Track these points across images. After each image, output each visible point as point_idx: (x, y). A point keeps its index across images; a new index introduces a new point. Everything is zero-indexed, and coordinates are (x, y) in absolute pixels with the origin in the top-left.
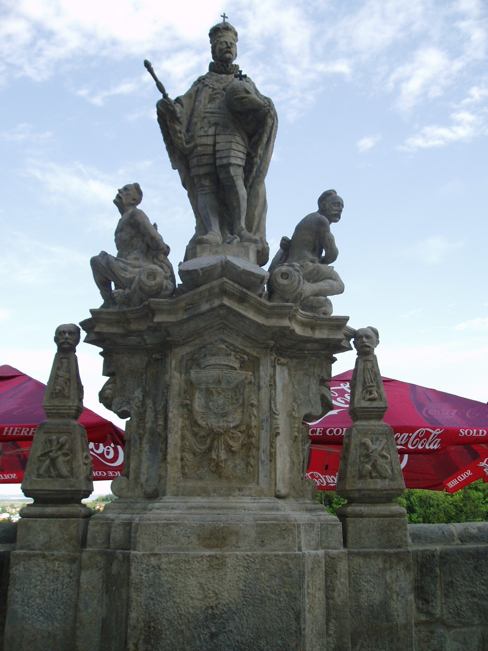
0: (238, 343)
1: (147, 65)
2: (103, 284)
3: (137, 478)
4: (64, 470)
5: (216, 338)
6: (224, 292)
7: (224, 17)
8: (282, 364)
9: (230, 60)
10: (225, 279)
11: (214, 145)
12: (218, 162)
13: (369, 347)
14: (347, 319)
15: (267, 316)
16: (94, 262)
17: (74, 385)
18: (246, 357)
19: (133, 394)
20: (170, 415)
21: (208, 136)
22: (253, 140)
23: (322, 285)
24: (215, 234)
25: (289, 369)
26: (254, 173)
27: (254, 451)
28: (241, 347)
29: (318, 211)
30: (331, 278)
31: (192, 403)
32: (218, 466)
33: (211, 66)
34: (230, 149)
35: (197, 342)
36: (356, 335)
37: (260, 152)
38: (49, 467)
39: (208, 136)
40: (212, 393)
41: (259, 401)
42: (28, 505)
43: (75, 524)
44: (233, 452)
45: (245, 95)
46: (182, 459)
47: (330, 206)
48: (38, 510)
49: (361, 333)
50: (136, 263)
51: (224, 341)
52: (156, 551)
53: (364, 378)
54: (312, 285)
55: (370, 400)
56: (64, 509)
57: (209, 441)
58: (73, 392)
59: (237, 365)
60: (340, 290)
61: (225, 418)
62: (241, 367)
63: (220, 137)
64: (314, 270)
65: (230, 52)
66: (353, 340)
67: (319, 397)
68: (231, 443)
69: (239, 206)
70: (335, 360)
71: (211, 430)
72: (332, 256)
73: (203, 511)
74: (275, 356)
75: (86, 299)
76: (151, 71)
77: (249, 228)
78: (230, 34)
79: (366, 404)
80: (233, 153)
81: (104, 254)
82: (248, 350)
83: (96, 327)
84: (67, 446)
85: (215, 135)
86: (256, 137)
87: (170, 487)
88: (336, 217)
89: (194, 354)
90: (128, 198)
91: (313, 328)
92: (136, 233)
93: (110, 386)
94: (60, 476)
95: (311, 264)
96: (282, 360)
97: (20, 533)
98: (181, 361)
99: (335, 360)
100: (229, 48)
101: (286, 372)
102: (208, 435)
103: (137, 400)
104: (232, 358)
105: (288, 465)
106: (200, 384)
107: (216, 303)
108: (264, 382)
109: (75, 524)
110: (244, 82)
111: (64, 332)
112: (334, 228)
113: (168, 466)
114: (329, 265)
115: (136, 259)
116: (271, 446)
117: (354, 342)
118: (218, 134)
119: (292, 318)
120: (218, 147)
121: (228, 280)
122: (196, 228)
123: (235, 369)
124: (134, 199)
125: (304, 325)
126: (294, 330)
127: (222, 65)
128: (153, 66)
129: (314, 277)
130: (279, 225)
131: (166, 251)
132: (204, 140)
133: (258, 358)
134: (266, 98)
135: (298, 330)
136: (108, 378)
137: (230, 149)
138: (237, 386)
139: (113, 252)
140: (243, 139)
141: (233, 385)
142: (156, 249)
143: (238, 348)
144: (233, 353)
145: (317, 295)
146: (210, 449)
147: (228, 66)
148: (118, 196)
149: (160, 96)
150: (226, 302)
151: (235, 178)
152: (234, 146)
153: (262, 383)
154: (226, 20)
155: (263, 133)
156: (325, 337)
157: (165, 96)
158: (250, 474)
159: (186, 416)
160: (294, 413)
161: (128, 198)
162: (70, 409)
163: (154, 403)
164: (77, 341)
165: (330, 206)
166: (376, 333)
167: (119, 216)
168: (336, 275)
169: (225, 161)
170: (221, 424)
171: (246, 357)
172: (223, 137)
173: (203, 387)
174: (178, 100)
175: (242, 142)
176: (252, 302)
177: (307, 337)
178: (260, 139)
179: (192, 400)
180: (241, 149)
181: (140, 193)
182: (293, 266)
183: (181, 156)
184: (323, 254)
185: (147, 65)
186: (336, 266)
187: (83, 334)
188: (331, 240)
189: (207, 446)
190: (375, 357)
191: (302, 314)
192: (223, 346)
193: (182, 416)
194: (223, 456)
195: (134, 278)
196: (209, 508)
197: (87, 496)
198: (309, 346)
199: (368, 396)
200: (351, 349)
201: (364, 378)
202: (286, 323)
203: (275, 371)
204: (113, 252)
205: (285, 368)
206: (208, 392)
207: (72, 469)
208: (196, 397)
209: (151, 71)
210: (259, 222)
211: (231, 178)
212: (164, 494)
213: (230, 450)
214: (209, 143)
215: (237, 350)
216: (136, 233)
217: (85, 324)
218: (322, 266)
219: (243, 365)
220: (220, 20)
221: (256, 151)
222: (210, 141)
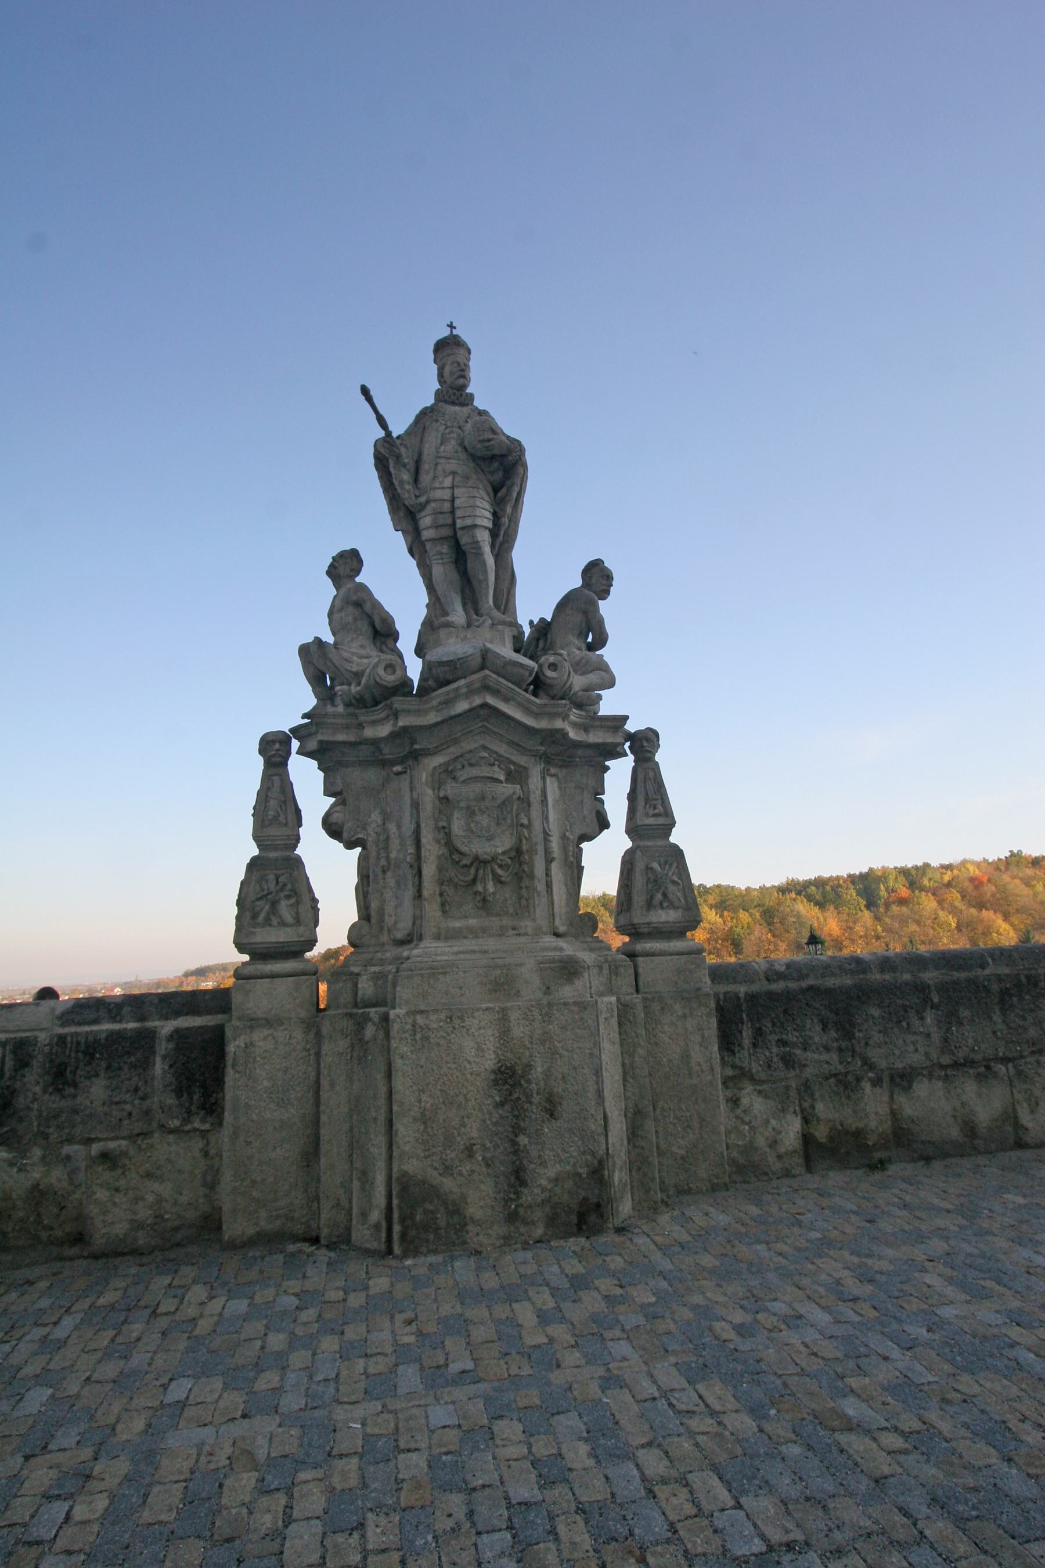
0: (502, 749)
1: (365, 391)
2: (316, 678)
3: (381, 920)
4: (289, 918)
5: (476, 745)
6: (486, 688)
7: (451, 326)
8: (552, 776)
9: (464, 387)
10: (487, 672)
11: (453, 501)
12: (459, 523)
13: (650, 752)
14: (626, 718)
15: (537, 716)
16: (305, 651)
17: (291, 810)
18: (512, 767)
19: (369, 817)
20: (424, 841)
21: (444, 488)
22: (499, 494)
23: (593, 678)
24: (458, 615)
25: (559, 782)
26: (501, 538)
27: (526, 882)
28: (505, 755)
29: (583, 586)
30: (600, 669)
31: (449, 824)
32: (484, 900)
33: (438, 393)
34: (475, 507)
35: (452, 749)
36: (630, 737)
37: (509, 510)
38: (268, 914)
39: (444, 488)
40: (473, 813)
41: (529, 820)
42: (243, 963)
43: (307, 983)
44: (501, 882)
45: (492, 436)
46: (441, 895)
47: (597, 578)
48: (251, 969)
49: (640, 736)
50: (363, 652)
51: (485, 748)
52: (422, 1008)
53: (646, 790)
54: (581, 677)
55: (655, 815)
56: (289, 965)
57: (473, 871)
58: (291, 818)
59: (502, 778)
60: (611, 683)
61: (492, 843)
62: (506, 779)
63: (460, 489)
64: (582, 658)
65: (464, 377)
66: (628, 744)
67: (594, 814)
68: (499, 871)
69: (486, 579)
70: (607, 768)
71: (476, 858)
72: (601, 641)
73: (473, 957)
74: (543, 765)
75: (293, 701)
76: (369, 399)
77: (497, 606)
78: (462, 351)
79: (651, 821)
80: (478, 512)
81: (318, 641)
82: (514, 758)
83: (315, 736)
84: (289, 887)
85: (453, 488)
86: (504, 490)
87: (429, 929)
88: (604, 593)
89: (449, 765)
90: (345, 567)
91: (586, 729)
92: (360, 614)
93: (338, 808)
94: (283, 924)
95: (578, 652)
96: (553, 771)
97: (237, 999)
98: (432, 775)
99: (607, 768)
100: (463, 370)
101: (556, 784)
102: (472, 864)
103: (374, 825)
104: (496, 768)
105: (564, 896)
106: (458, 802)
107: (477, 701)
108: (535, 797)
109: (307, 983)
110: (484, 418)
111: (274, 742)
112: (604, 607)
113: (426, 904)
114: (598, 653)
115: (362, 646)
116: (547, 875)
117: (630, 747)
118: (458, 487)
119: (566, 717)
120: (457, 502)
121: (491, 674)
122: (428, 606)
123: (501, 782)
124: (352, 570)
125: (575, 725)
126: (567, 733)
127: (454, 394)
128: (373, 393)
129: (582, 667)
130: (535, 602)
131: (395, 636)
132: (438, 494)
133: (525, 768)
134: (515, 440)
135: (572, 734)
136: (332, 800)
137: (475, 507)
138: (503, 803)
139: (329, 638)
140: (488, 494)
141: (499, 802)
142: (384, 632)
143: (501, 756)
144: (497, 763)
145: (586, 690)
146: (474, 881)
147: (461, 395)
148: (332, 566)
149: (382, 434)
150: (491, 700)
151: (481, 544)
152: (478, 503)
153: (532, 799)
154: (455, 332)
155: (512, 485)
156: (600, 741)
157: (388, 434)
158: (523, 907)
159: (443, 842)
160: (567, 834)
161: (345, 567)
162: (289, 839)
163: (399, 827)
164: (289, 753)
165: (597, 578)
166: (657, 735)
167: (334, 592)
168: (607, 665)
169: (468, 522)
170: (488, 850)
171: (512, 767)
172: (464, 490)
173: (463, 804)
174: (398, 437)
175: (487, 498)
176: (519, 700)
177: (580, 742)
178: (509, 491)
179: (449, 821)
180: (487, 506)
181: (360, 562)
182: (561, 655)
183: (405, 514)
184: (590, 640)
185: (365, 391)
186: (606, 653)
187: (295, 744)
188: (601, 622)
189: (472, 877)
190: (657, 764)
191: (575, 715)
192: (486, 755)
193: (438, 842)
194: (491, 888)
195: (363, 672)
196: (480, 952)
197: (311, 950)
198: (580, 752)
199: (651, 812)
200: (626, 755)
201: (646, 790)
202: (559, 724)
203: (545, 783)
204: (329, 638)
205: (554, 779)
206: (470, 813)
207: (297, 913)
208: (455, 816)
209: (369, 399)
210: (507, 600)
211: (476, 545)
212: (421, 938)
213: (498, 880)
214: (445, 498)
215: (500, 760)
216: (360, 614)
217: (296, 731)
218: (590, 654)
219: (510, 777)
220: (446, 332)
221: (504, 510)
222: (446, 494)
